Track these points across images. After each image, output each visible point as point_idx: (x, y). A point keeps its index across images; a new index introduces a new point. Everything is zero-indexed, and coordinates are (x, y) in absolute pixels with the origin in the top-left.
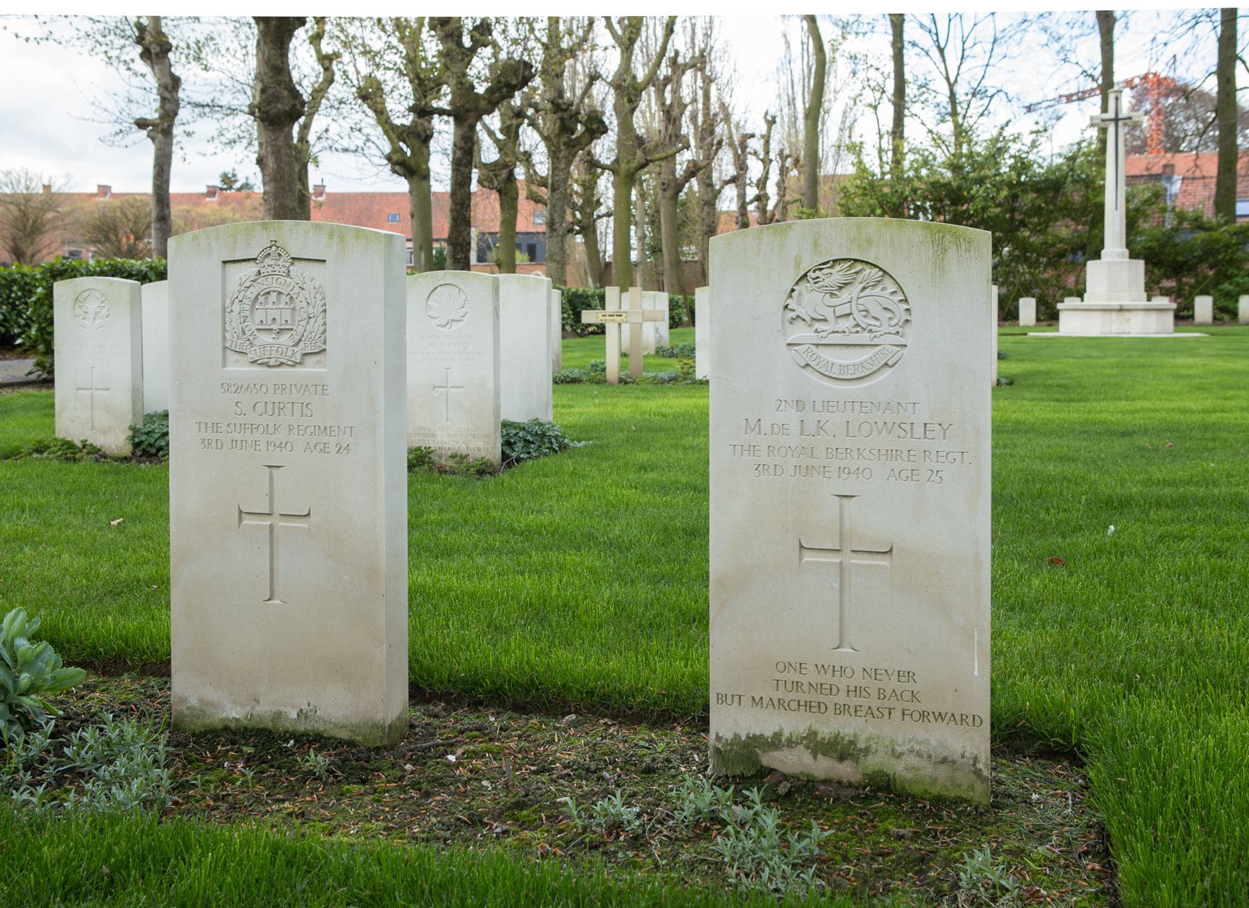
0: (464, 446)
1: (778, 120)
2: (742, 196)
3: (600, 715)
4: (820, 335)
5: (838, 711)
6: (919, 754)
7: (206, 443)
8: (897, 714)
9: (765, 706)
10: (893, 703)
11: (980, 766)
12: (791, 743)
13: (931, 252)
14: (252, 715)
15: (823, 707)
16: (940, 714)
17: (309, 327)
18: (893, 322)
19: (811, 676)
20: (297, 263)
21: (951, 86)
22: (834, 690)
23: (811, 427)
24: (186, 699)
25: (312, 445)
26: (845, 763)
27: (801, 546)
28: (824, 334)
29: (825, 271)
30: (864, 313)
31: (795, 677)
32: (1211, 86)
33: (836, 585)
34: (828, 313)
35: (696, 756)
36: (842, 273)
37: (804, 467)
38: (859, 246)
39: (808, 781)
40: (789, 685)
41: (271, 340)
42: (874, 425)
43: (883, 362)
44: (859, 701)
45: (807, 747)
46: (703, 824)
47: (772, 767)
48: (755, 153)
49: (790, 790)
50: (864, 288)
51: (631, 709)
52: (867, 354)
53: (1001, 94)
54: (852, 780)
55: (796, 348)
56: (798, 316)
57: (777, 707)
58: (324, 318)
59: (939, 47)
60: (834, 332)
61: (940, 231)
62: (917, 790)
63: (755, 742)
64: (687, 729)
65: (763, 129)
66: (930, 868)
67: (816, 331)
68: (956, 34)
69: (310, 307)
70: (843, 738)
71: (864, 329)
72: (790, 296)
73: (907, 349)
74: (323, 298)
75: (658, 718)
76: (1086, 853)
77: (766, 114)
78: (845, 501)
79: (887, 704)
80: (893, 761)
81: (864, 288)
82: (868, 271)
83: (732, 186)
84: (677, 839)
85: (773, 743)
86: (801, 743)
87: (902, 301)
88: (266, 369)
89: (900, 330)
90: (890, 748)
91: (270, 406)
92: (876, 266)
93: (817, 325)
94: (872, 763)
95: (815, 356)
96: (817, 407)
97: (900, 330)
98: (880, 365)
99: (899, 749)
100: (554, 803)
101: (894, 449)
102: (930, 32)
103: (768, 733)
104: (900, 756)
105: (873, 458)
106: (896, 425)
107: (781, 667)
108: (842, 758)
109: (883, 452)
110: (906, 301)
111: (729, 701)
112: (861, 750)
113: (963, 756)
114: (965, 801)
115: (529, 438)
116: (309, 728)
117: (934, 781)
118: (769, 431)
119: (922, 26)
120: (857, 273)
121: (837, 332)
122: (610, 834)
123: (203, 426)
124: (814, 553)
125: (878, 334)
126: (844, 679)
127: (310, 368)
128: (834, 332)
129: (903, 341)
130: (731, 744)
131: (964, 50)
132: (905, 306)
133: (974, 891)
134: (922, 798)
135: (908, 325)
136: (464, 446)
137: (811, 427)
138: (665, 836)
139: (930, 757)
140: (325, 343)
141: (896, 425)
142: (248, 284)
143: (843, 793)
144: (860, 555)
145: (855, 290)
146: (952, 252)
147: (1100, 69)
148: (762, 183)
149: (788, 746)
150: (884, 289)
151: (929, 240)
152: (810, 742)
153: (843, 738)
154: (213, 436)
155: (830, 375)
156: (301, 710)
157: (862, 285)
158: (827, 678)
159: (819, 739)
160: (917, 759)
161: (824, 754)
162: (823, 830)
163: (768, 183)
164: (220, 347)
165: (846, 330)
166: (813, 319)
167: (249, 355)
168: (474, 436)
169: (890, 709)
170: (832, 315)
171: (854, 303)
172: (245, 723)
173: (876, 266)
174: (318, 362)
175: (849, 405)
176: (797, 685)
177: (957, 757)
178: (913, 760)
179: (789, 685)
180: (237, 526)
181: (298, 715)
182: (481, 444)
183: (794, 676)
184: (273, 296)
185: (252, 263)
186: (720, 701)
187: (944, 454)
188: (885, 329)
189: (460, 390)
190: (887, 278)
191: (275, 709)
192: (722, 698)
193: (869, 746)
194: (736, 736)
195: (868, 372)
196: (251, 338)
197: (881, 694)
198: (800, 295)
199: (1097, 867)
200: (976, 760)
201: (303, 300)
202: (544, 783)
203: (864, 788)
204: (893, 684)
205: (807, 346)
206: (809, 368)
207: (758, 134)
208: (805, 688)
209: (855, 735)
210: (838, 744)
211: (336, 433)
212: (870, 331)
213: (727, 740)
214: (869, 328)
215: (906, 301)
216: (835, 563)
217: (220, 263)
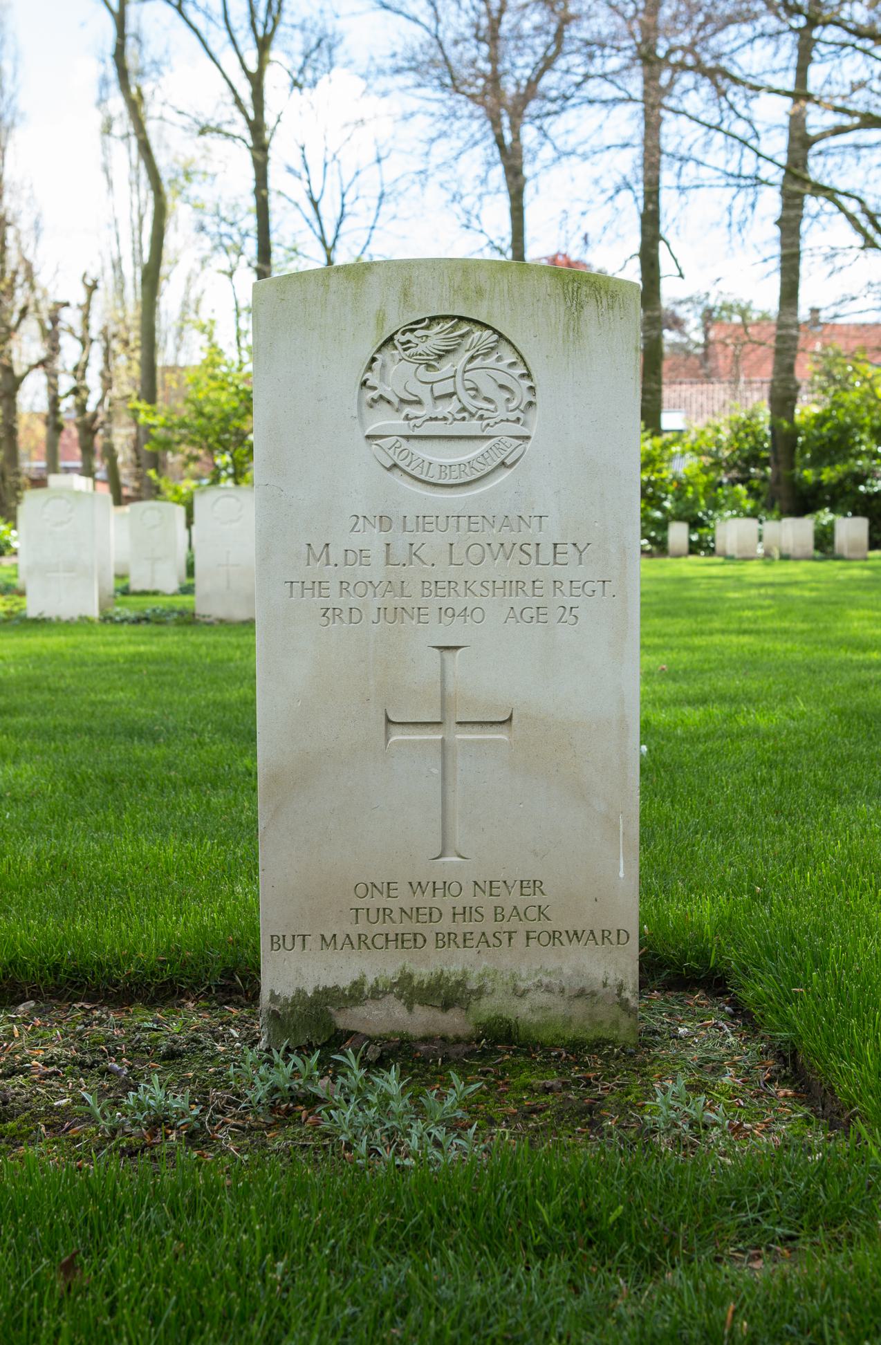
1: (100, 284)
2: (53, 387)
3: (69, 999)
4: (412, 423)
5: (440, 943)
6: (549, 989)
8: (519, 939)
9: (339, 946)
10: (514, 924)
11: (627, 994)
12: (377, 993)
13: (562, 309)
15: (420, 940)
16: (576, 933)
18: (512, 405)
19: (404, 899)
22: (436, 916)
23: (400, 553)
26: (451, 1012)
27: (388, 721)
28: (418, 422)
29: (419, 333)
30: (472, 393)
31: (381, 901)
32: (633, 273)
33: (437, 771)
34: (424, 393)
35: (232, 1031)
36: (442, 336)
37: (390, 611)
38: (466, 299)
39: (402, 1042)
40: (373, 914)
42: (486, 547)
43: (499, 460)
44: (468, 927)
45: (399, 997)
46: (283, 1106)
47: (351, 1029)
48: (71, 331)
49: (381, 1055)
50: (473, 358)
51: (115, 986)
52: (474, 451)
54: (461, 1033)
55: (379, 442)
56: (381, 397)
57: (356, 946)
59: (312, 199)
60: (431, 419)
61: (574, 281)
62: (545, 1036)
63: (328, 997)
64: (203, 1003)
65: (81, 297)
66: (603, 1118)
67: (407, 418)
68: (333, 181)
70: (448, 979)
71: (472, 415)
72: (369, 368)
73: (531, 441)
75: (157, 995)
76: (770, 1081)
77: (85, 275)
78: (447, 654)
79: (506, 926)
80: (515, 1001)
81: (473, 358)
82: (478, 334)
83: (41, 370)
84: (252, 1128)
85: (351, 997)
86: (391, 992)
87: (522, 376)
89: (521, 415)
90: (511, 985)
92: (487, 327)
93: (408, 410)
94: (487, 1008)
95: (405, 453)
96: (408, 524)
97: (521, 415)
98: (495, 464)
99: (522, 985)
100: (52, 1108)
101: (514, 579)
103: (345, 983)
104: (523, 995)
105: (485, 592)
106: (517, 547)
107: (361, 890)
108: (446, 1006)
109: (499, 584)
110: (528, 375)
111: (289, 945)
112: (472, 992)
113: (605, 985)
114: (609, 1042)
117: (568, 1022)
118: (341, 560)
119: (290, 170)
120: (462, 336)
121: (436, 419)
122: (153, 1135)
124: (405, 729)
125: (491, 422)
126: (448, 897)
128: (431, 419)
129: (525, 432)
130: (293, 1005)
131: (343, 206)
132: (528, 383)
133: (676, 1131)
134: (553, 1045)
135: (531, 411)
137: (400, 553)
138: (234, 1126)
139: (562, 991)
141: (517, 547)
143: (453, 1050)
144: (469, 728)
145: (460, 359)
146: (590, 310)
147: (509, 239)
148: (80, 370)
149: (373, 998)
150: (499, 359)
151: (560, 291)
152: (404, 989)
153: (448, 979)
155: (427, 479)
157: (469, 354)
158: (425, 900)
159: (415, 984)
160: (547, 995)
161: (421, 1004)
162: (467, 1084)
163: (89, 371)
165: (449, 416)
166: (402, 401)
169: (510, 933)
170: (429, 395)
171: (459, 378)
173: (487, 327)
175: (452, 521)
176: (385, 913)
177: (597, 987)
178: (541, 998)
179: (373, 914)
183: (380, 901)
186: (276, 946)
187: (581, 584)
188: (502, 413)
190: (504, 345)
192: (278, 942)
193: (483, 986)
194: (300, 992)
195: (479, 475)
197: (498, 913)
198: (383, 366)
199: (790, 1093)
200: (621, 987)
202: (22, 1087)
203: (478, 1041)
204: (514, 898)
205: (393, 439)
206: (396, 471)
207: (73, 303)
208: (396, 916)
209: (465, 973)
210: (441, 987)
212: (481, 418)
213: (286, 999)
214: (480, 412)
215: (528, 375)
216: (435, 741)
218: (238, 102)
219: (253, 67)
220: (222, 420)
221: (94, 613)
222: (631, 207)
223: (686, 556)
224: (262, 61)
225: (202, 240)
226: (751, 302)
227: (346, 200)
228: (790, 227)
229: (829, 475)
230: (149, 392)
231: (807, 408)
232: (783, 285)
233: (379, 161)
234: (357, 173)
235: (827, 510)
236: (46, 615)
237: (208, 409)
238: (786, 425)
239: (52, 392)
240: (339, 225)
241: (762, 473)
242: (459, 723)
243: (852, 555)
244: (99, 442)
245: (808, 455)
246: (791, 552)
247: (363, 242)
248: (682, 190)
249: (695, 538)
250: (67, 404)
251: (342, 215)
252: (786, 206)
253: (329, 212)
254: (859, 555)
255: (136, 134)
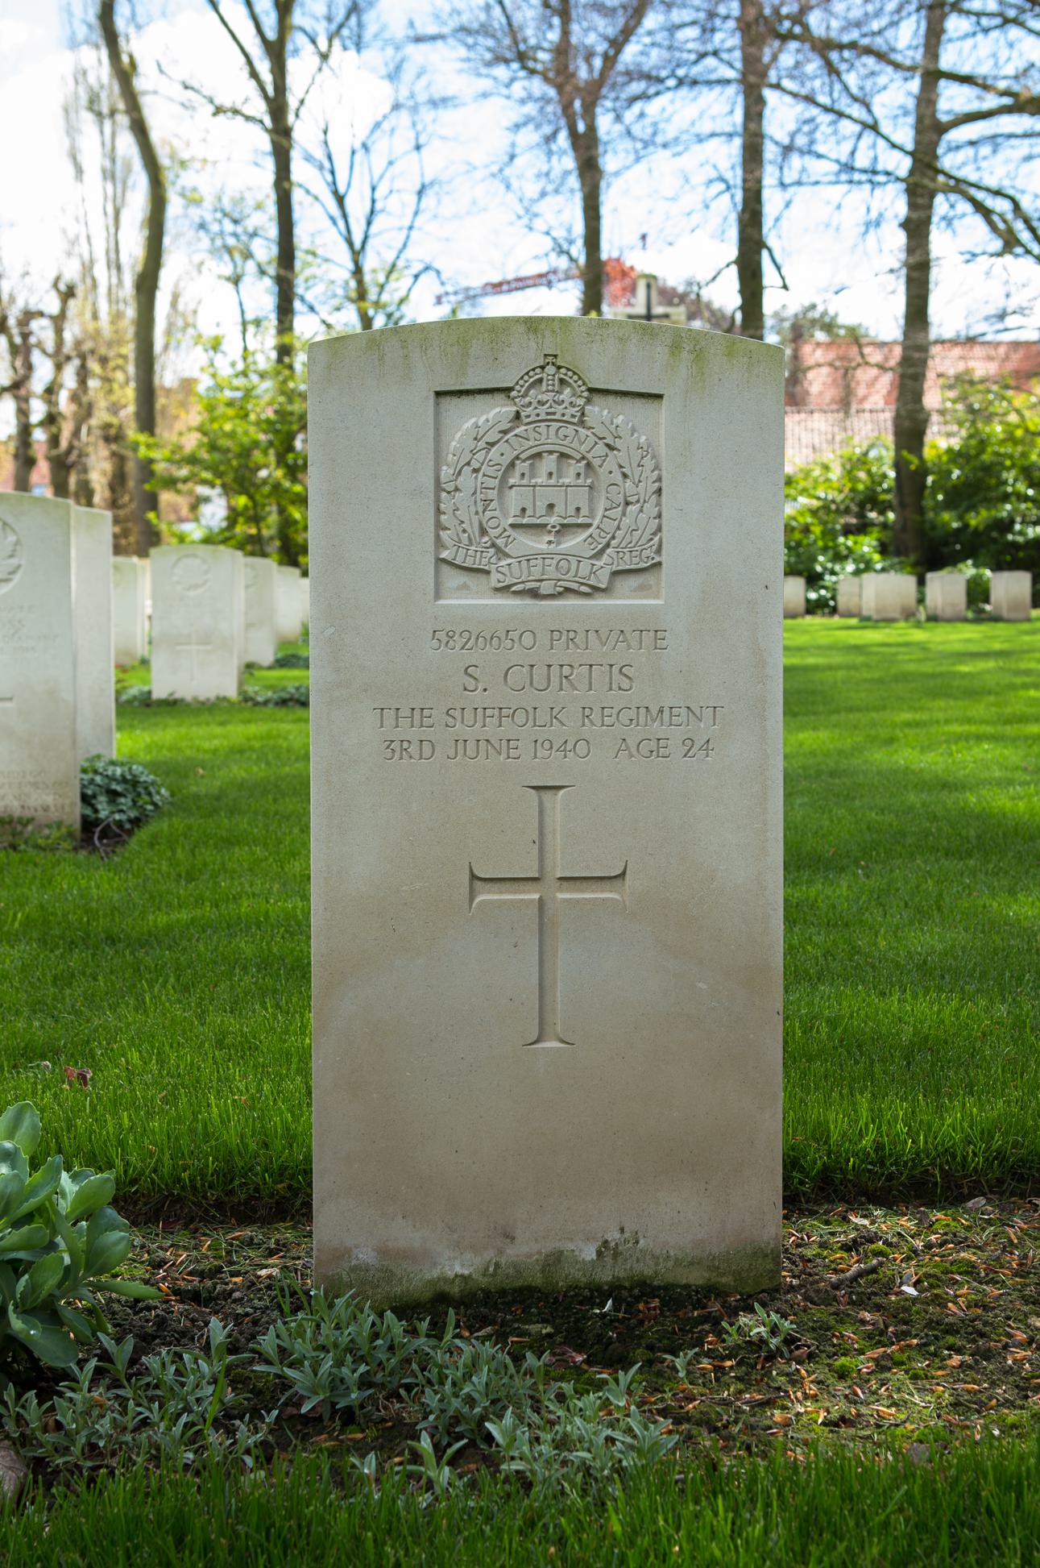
0: (16, 804)
1: (80, 291)
7: (395, 748)
14: (497, 1265)
17: (626, 521)
20: (597, 398)
21: (357, 254)
24: (348, 1251)
25: (632, 743)
41: (544, 546)
53: (432, 274)
58: (659, 504)
59: (336, 193)
65: (53, 306)
69: (629, 483)
74: (657, 467)
88: (528, 601)
91: (539, 673)
102: (321, 167)
115: (114, 786)
116: (622, 1274)
123: (389, 715)
127: (625, 600)
131: (373, 201)
136: (16, 804)
140: (659, 551)
142: (493, 436)
154: (414, 734)
156: (606, 1242)
164: (430, 559)
167: (495, 576)
168: (35, 785)
172: (484, 1282)
174: (643, 589)
180: (466, 906)
181: (599, 1253)
182: (49, 800)
184: (549, 463)
185: (499, 397)
189: (8, 705)
191: (548, 1246)
196: (500, 542)
201: (615, 468)
211: (683, 719)
217: (432, 395)
218: (254, 74)
219: (271, 34)
220: (239, 456)
221: (232, 692)
222: (727, 209)
223: (803, 616)
224: (284, 26)
225: (199, 240)
226: (836, 315)
227: (377, 195)
228: (917, 229)
229: (977, 519)
230: (147, 419)
231: (940, 441)
232: (909, 304)
233: (418, 148)
234: (391, 163)
235: (970, 562)
236: (178, 696)
237: (224, 443)
238: (915, 461)
239: (23, 419)
240: (369, 223)
241: (882, 519)
242: (560, 879)
243: (1013, 615)
244: (73, 480)
245: (940, 497)
246: (939, 612)
247: (399, 245)
248: (783, 185)
249: (813, 596)
250: (39, 435)
251: (372, 212)
252: (912, 206)
253: (357, 207)
254: (1021, 615)
255: (128, 112)
